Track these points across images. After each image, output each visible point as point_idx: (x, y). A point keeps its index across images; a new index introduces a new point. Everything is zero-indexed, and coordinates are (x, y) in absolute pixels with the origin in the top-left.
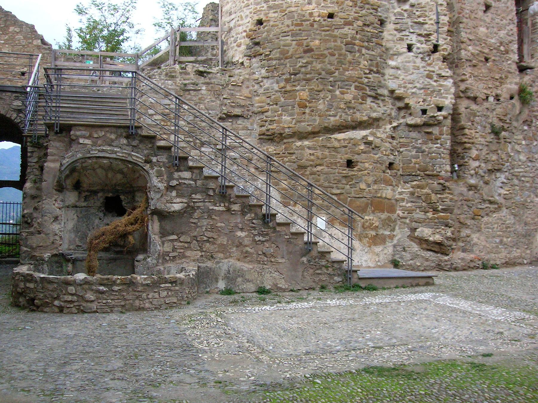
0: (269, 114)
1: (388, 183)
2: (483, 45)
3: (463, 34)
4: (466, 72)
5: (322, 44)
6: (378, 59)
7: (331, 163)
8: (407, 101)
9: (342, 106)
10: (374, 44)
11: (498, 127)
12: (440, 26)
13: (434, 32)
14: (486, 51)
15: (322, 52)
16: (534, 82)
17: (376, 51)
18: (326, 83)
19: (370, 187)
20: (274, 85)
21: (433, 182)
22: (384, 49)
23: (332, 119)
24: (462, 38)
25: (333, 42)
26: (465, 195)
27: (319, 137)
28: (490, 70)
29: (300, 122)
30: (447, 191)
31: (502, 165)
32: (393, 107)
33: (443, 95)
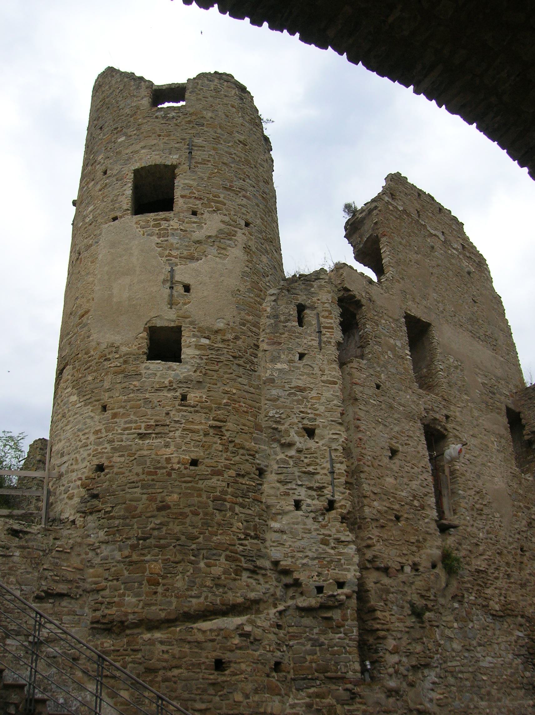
0: (107, 592)
1: (273, 691)
2: (392, 499)
3: (365, 486)
4: (373, 534)
5: (182, 499)
6: (257, 519)
7: (193, 665)
8: (296, 575)
9: (209, 583)
10: (251, 500)
11: (420, 606)
12: (335, 476)
13: (328, 484)
14: (396, 507)
15: (181, 511)
16: (460, 544)
17: (253, 509)
18: (187, 551)
19: (249, 698)
20: (116, 552)
21: (337, 687)
22: (264, 507)
23: (194, 601)
24: (364, 492)
25: (197, 497)
26: (384, 704)
27: (176, 626)
28: (403, 531)
29: (150, 605)
30: (358, 700)
31: (430, 658)
32: (278, 584)
33: (344, 567)
